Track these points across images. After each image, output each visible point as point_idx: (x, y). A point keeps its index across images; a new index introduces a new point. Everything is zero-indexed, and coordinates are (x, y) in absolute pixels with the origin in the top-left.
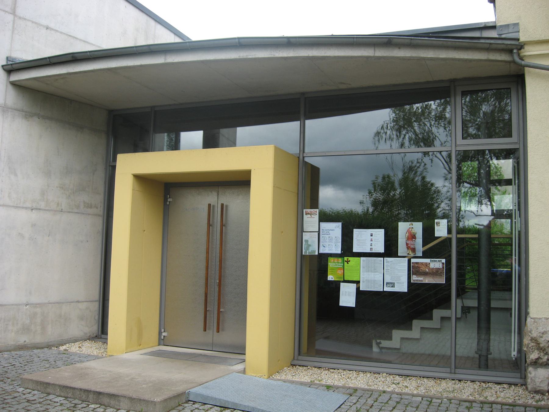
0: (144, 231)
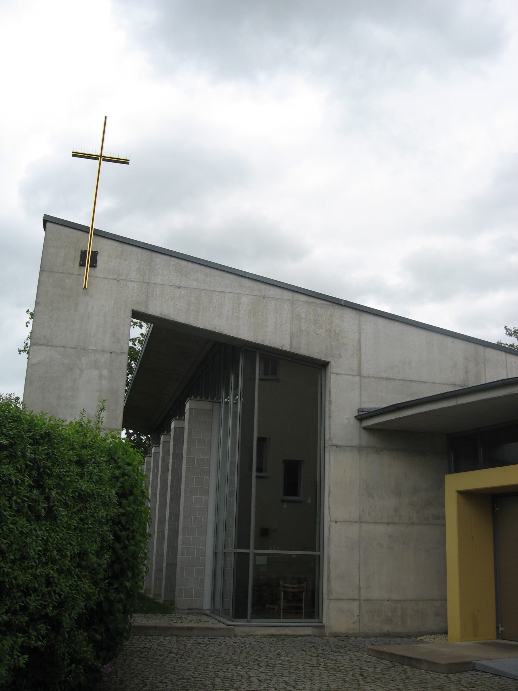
0: (473, 537)
